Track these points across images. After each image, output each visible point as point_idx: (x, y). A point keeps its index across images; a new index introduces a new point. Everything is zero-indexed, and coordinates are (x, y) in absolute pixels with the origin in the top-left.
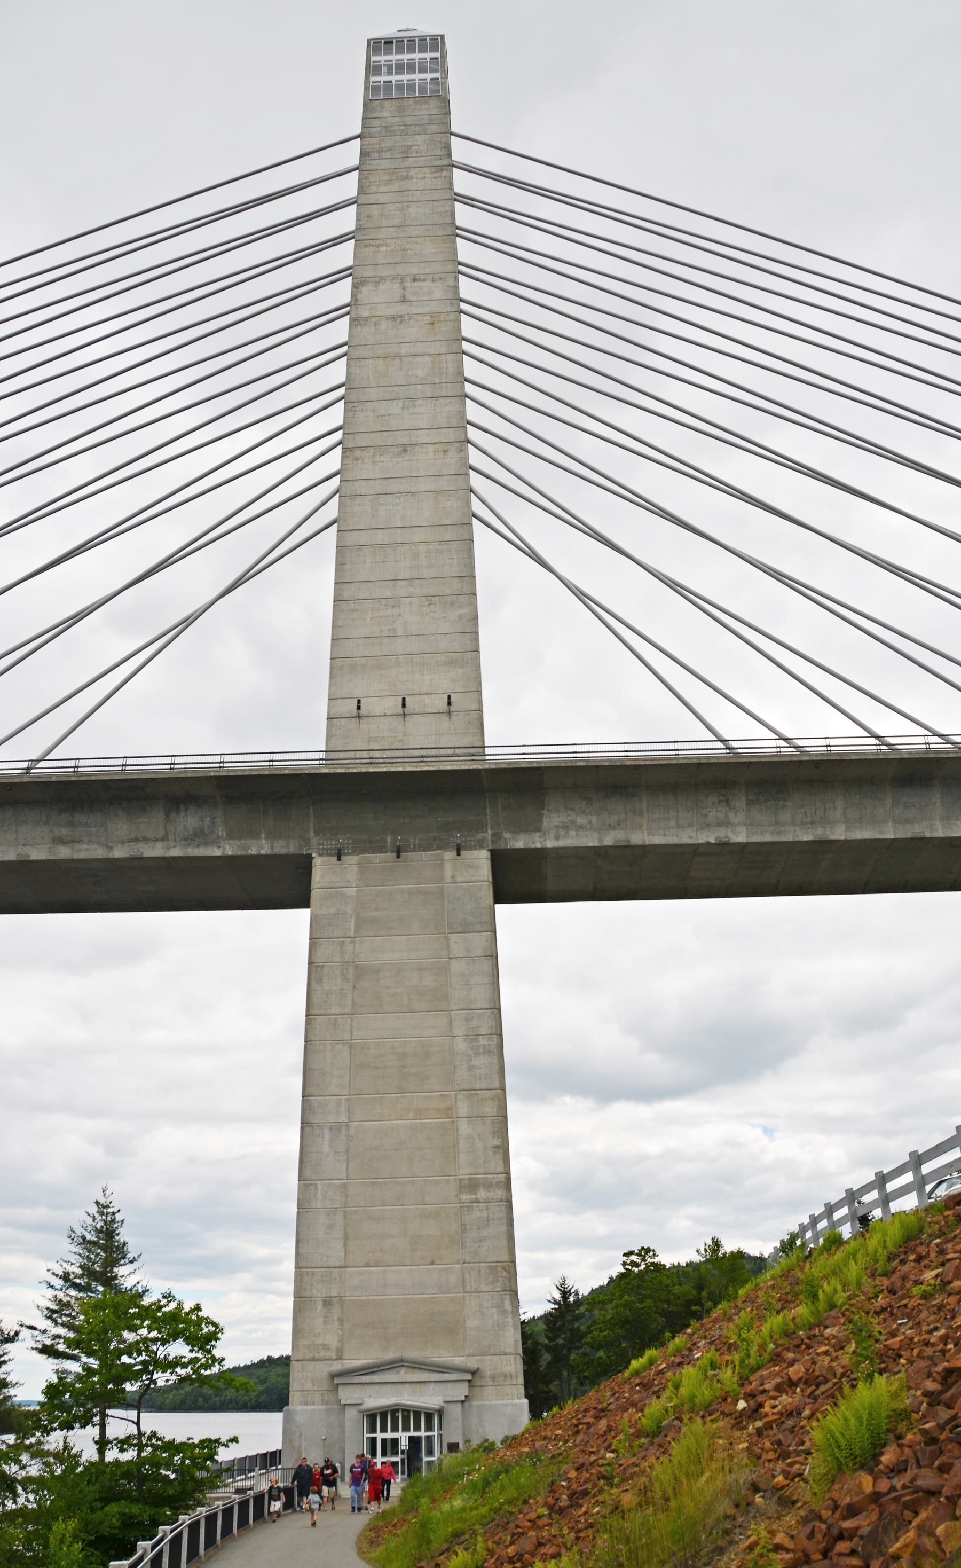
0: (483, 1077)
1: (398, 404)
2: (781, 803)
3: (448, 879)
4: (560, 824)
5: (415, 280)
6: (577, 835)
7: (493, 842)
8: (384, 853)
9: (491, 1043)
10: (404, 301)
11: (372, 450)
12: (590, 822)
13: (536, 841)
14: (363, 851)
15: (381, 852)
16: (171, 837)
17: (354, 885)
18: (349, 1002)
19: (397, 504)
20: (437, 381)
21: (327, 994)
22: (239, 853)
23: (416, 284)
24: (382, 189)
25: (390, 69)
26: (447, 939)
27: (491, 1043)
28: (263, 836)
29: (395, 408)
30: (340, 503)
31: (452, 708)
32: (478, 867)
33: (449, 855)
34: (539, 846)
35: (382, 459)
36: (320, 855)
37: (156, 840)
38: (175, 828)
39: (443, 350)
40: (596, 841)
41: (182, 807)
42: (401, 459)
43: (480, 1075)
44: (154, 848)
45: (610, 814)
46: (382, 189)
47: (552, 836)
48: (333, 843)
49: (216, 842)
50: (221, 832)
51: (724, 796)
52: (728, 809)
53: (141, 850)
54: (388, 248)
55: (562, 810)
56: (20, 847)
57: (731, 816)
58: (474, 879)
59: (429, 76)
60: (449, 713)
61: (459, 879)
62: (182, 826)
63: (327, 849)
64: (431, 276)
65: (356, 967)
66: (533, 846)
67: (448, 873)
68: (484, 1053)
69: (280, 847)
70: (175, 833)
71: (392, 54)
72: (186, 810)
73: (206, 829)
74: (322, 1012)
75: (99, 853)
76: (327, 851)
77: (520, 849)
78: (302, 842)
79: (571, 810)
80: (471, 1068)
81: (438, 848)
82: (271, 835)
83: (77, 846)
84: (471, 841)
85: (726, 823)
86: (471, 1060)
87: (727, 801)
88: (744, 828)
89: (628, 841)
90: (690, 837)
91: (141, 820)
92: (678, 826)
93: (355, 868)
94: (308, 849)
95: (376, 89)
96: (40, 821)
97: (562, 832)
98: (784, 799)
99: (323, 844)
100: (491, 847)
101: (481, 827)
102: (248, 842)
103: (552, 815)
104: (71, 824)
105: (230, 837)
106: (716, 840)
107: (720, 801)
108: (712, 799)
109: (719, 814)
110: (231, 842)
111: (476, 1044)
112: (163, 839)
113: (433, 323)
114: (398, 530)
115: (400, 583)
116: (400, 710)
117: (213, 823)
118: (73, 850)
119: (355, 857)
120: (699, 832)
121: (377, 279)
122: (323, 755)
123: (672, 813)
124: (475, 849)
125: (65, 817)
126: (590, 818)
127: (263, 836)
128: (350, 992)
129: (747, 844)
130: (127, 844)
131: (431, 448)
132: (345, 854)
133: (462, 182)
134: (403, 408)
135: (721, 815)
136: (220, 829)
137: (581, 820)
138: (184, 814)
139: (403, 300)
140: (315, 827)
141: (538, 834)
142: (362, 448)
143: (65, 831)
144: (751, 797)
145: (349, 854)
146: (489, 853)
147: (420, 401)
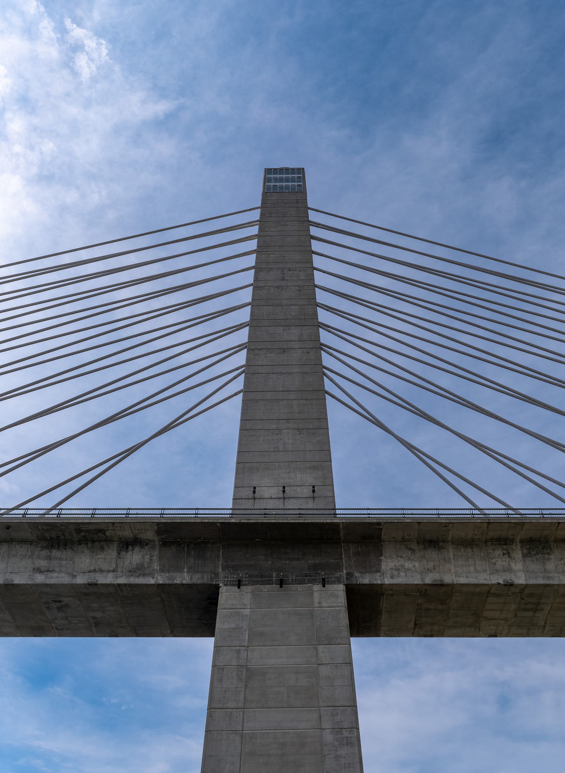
0: (347, 766)
1: (280, 328)
2: (547, 556)
3: (317, 605)
4: (393, 567)
5: (289, 270)
6: (406, 576)
7: (347, 579)
8: (271, 584)
9: (352, 735)
10: (284, 280)
11: (265, 351)
12: (414, 566)
13: (377, 580)
14: (256, 583)
15: (269, 584)
16: (119, 570)
17: (249, 607)
18: (242, 699)
19: (279, 379)
20: (302, 317)
21: (225, 691)
22: (167, 582)
23: (290, 272)
24: (271, 229)
25: (276, 180)
26: (316, 649)
27: (352, 735)
28: (185, 570)
29: (280, 330)
30: (246, 378)
31: (315, 495)
32: (337, 596)
33: (317, 587)
34: (380, 582)
35: (270, 355)
36: (225, 585)
37: (109, 571)
38: (124, 563)
39: (306, 303)
40: (420, 580)
41: (130, 548)
42: (282, 356)
43: (345, 764)
44: (106, 577)
45: (428, 561)
46: (271, 229)
47: (388, 575)
48: (235, 576)
49: (151, 575)
50: (156, 566)
51: (506, 550)
52: (509, 560)
53: (97, 578)
54: (275, 256)
55: (395, 557)
56: (8, 574)
57: (513, 565)
58: (334, 604)
59: (296, 184)
60: (314, 498)
61: (324, 604)
62: (128, 561)
63: (230, 581)
64: (299, 269)
65: (248, 670)
66: (376, 583)
67: (316, 600)
68: (347, 744)
69: (197, 579)
70: (123, 567)
71: (277, 182)
72: (133, 550)
73: (145, 564)
74: (220, 706)
75: (65, 579)
76: (230, 582)
77: (366, 584)
78: (213, 576)
79: (401, 557)
80: (337, 757)
81: (309, 582)
82: (192, 570)
83: (50, 574)
84: (332, 578)
85: (509, 570)
86: (337, 750)
87: (509, 553)
88: (523, 574)
89: (442, 581)
90: (485, 579)
91: (100, 556)
92: (476, 571)
93: (250, 595)
94: (217, 581)
95: (269, 188)
96: (26, 555)
97: (395, 573)
98: (549, 554)
99: (227, 577)
100: (346, 583)
101: (338, 567)
102: (175, 574)
103: (388, 560)
104: (49, 558)
105: (162, 570)
106: (504, 581)
107: (504, 554)
108: (498, 552)
109: (504, 563)
110: (162, 574)
111: (341, 736)
112: (113, 571)
113: (300, 290)
114: (281, 393)
115: (282, 421)
116: (281, 495)
117: (151, 560)
118: (46, 577)
119: (250, 587)
120: (491, 576)
121: (269, 269)
122: (231, 512)
123: (471, 562)
124: (335, 584)
125: (44, 553)
126: (414, 563)
127: (185, 570)
128: (243, 690)
129: (526, 586)
130: (87, 574)
131: (299, 351)
132: (243, 585)
133: (314, 231)
134: (283, 330)
135: (505, 564)
136: (156, 564)
137: (408, 565)
138: (131, 553)
139: (283, 279)
140: (222, 565)
141: (378, 574)
142: (260, 349)
143: (43, 563)
144: (525, 551)
145: (246, 585)
146: (345, 587)
147: (293, 327)
